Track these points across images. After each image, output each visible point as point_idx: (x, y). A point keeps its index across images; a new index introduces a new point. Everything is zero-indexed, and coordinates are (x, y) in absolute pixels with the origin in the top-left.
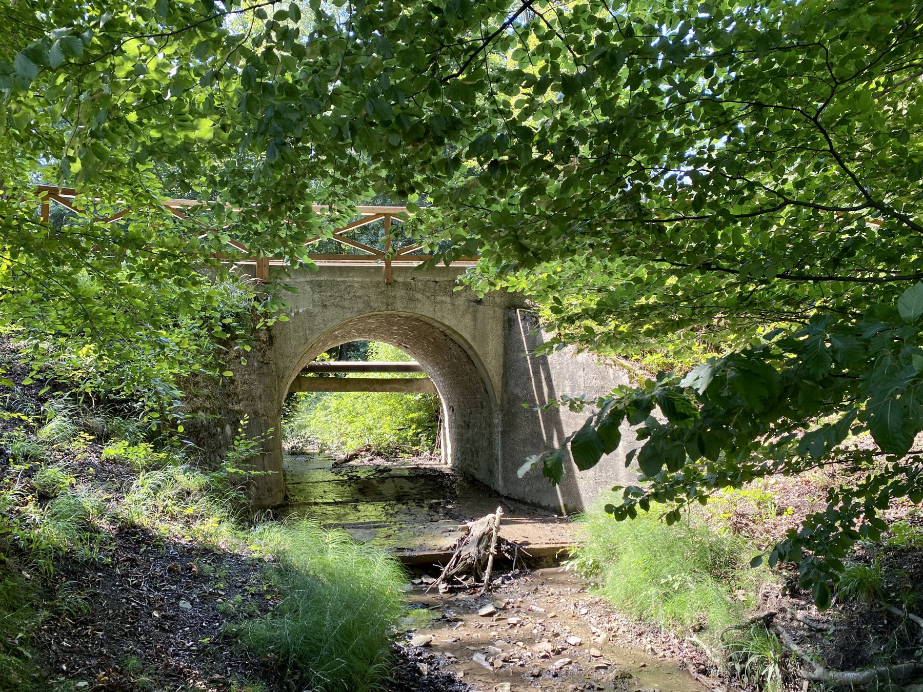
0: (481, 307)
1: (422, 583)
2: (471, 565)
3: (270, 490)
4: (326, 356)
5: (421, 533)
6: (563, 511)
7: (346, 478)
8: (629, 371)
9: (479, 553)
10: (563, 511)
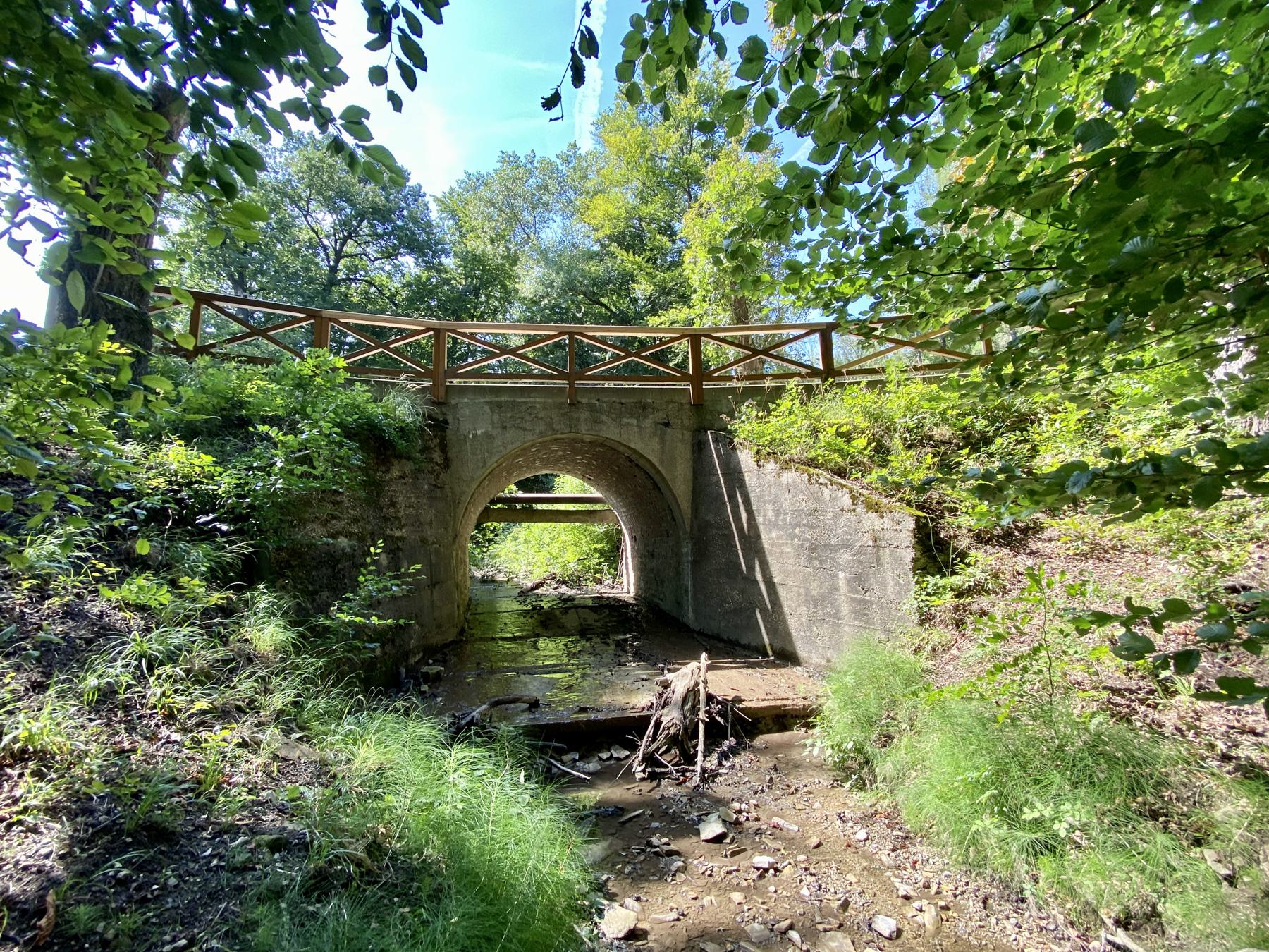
0: (669, 430)
1: (611, 757)
2: (675, 735)
3: (439, 626)
4: (513, 487)
5: (605, 686)
6: (770, 653)
7: (529, 607)
8: (851, 490)
9: (685, 718)
10: (770, 653)
